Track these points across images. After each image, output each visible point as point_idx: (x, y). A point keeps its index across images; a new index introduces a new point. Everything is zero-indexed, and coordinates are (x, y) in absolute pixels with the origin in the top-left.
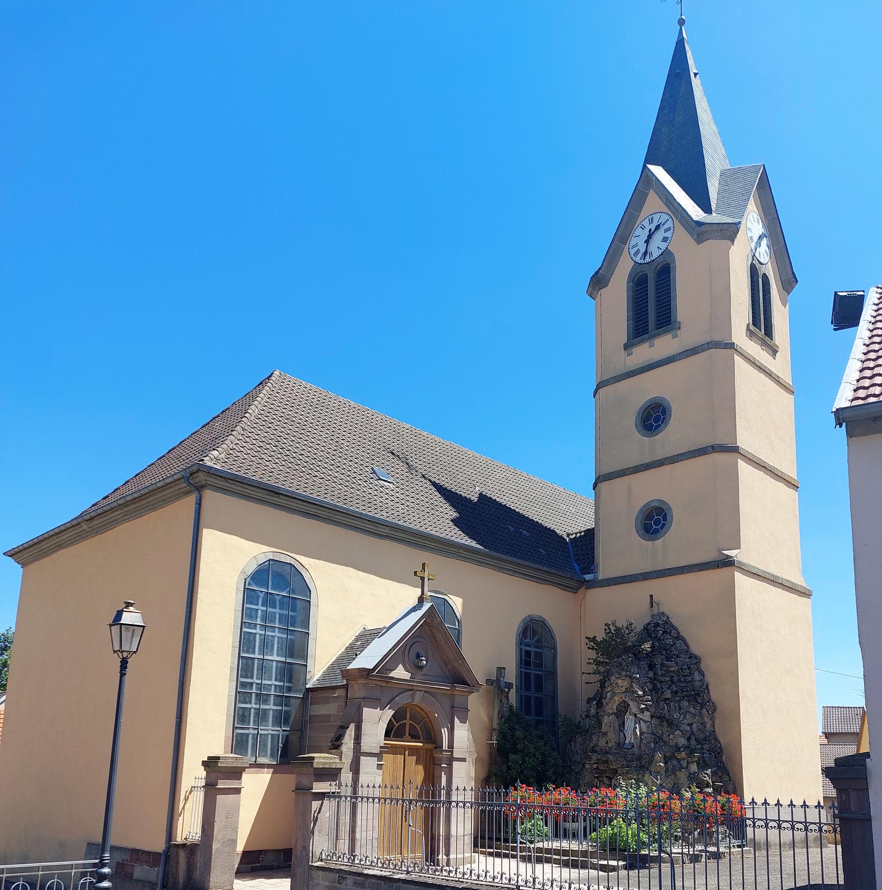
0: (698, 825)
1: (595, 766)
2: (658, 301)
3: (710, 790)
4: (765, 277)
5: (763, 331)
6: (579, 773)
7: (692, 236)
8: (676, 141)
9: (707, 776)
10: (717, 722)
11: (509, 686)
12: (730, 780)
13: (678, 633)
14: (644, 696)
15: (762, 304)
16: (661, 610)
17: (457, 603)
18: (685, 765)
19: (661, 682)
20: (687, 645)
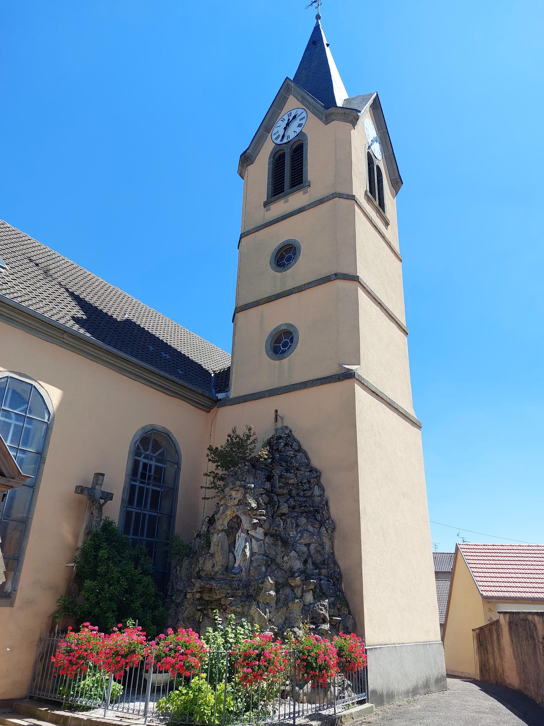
0: (310, 672)
1: (198, 596)
2: (292, 167)
3: (326, 627)
4: (378, 167)
5: (378, 202)
6: (179, 605)
7: (321, 119)
8: (312, 78)
9: (323, 608)
10: (336, 543)
11: (108, 496)
12: (350, 614)
13: (300, 446)
14: (257, 509)
15: (376, 181)
16: (285, 424)
17: (52, 395)
18: (299, 593)
19: (278, 495)
20: (308, 458)
